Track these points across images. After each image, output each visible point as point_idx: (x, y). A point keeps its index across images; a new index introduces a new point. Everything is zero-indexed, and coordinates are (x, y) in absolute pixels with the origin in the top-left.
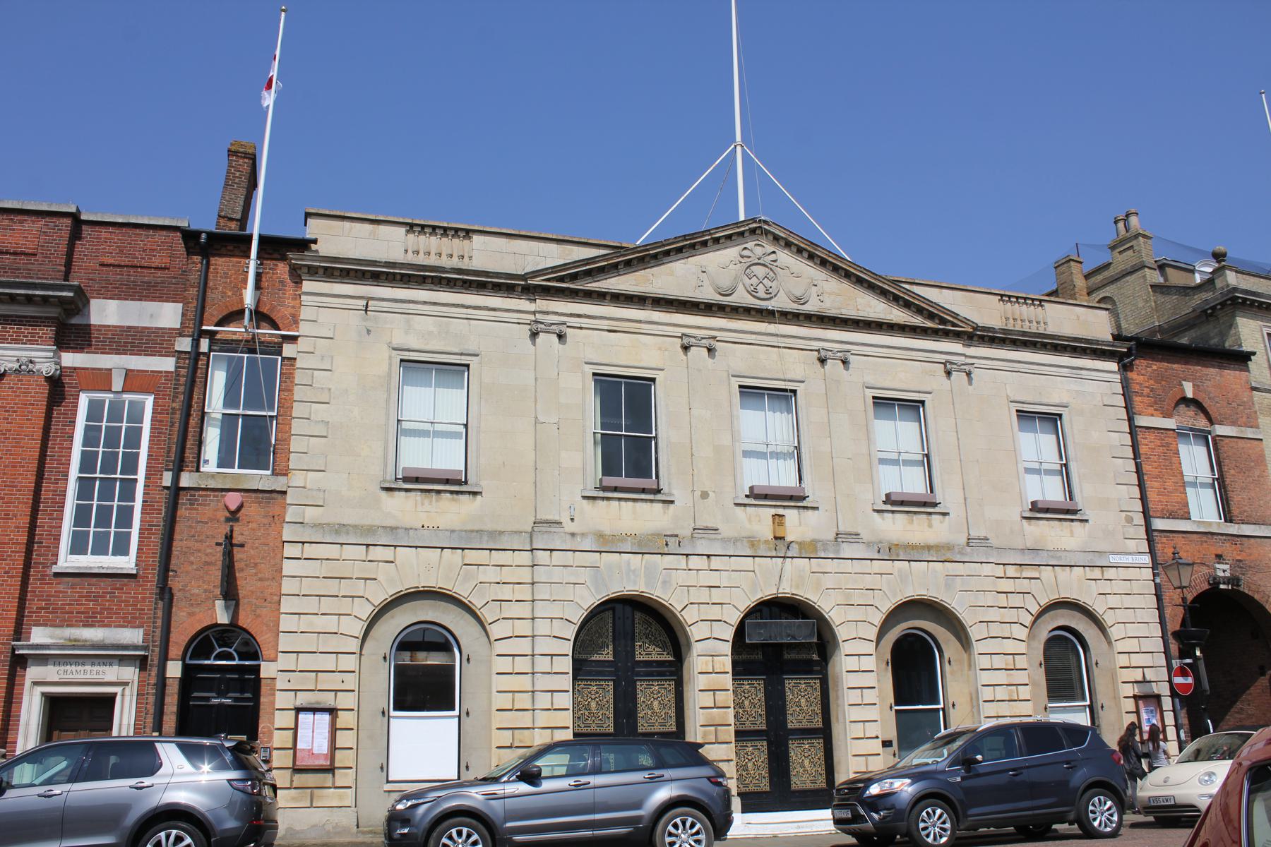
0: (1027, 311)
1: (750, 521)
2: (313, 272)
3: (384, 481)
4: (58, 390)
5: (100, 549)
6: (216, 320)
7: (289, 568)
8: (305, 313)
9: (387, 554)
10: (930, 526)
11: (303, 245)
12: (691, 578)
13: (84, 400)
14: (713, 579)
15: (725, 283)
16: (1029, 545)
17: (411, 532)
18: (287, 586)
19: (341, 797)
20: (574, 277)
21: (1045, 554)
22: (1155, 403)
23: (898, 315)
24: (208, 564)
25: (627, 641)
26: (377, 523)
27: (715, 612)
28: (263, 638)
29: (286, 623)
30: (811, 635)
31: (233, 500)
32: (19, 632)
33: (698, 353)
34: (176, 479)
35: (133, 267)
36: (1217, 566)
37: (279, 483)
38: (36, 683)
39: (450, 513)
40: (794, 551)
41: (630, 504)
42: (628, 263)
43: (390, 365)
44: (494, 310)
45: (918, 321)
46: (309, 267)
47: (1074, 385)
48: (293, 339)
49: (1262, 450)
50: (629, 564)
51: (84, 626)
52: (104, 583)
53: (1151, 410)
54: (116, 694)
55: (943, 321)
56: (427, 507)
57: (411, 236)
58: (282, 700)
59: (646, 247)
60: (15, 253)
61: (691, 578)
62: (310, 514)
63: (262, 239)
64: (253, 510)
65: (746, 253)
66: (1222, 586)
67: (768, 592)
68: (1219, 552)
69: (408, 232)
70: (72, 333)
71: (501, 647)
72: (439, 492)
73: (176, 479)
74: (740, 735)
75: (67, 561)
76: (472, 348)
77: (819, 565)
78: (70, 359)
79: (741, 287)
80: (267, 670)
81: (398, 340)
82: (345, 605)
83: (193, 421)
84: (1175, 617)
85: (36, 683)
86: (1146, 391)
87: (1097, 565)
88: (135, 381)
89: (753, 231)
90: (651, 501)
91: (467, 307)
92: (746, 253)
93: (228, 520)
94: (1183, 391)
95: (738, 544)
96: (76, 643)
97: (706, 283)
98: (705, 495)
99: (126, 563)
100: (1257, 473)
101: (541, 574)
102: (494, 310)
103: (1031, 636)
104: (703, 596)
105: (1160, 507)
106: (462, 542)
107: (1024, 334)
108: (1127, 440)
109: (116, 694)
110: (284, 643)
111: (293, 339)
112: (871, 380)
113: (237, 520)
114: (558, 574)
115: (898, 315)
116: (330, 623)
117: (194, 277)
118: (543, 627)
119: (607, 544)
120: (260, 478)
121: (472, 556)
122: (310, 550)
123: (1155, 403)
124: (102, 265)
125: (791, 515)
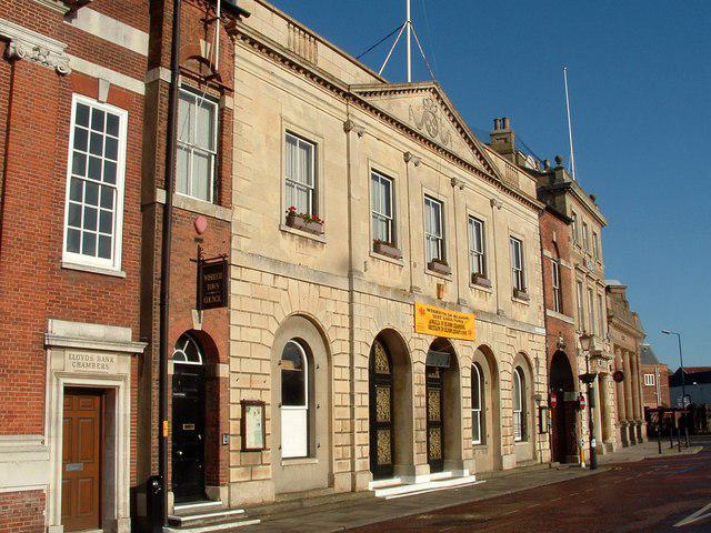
5: (89, 251)
19: (266, 472)
20: (365, 94)
24: (185, 276)
28: (219, 344)
29: (235, 333)
38: (60, 374)
45: (484, 169)
51: (88, 322)
52: (88, 275)
54: (119, 387)
55: (493, 173)
58: (235, 397)
80: (223, 371)
84: (550, 359)
87: (278, 266)
88: (117, 96)
99: (112, 265)
103: (278, 335)
109: (119, 387)
115: (478, 164)
120: (218, 212)
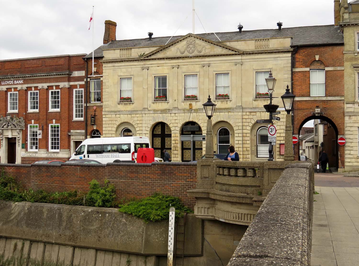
0: (263, 43)
1: (185, 105)
2: (104, 62)
3: (118, 102)
4: (71, 88)
6: (90, 74)
7: (104, 119)
8: (104, 71)
9: (119, 116)
10: (227, 104)
11: (102, 57)
12: (171, 118)
13: (74, 90)
14: (176, 118)
15: (182, 50)
16: (254, 107)
17: (122, 112)
18: (104, 123)
21: (258, 109)
22: (304, 63)
23: (225, 51)
25: (160, 131)
26: (117, 110)
27: (176, 125)
29: (104, 129)
30: (197, 129)
31: (95, 108)
32: (69, 131)
33: (176, 69)
34: (86, 105)
35: (79, 64)
36: (316, 109)
37: (101, 104)
39: (129, 107)
40: (193, 111)
41: (161, 103)
42: (164, 49)
43: (118, 80)
44: (136, 65)
46: (103, 62)
47: (275, 62)
48: (102, 77)
49: (343, 73)
50: (159, 116)
53: (302, 66)
56: (125, 106)
57: (121, 51)
59: (167, 45)
60: (61, 65)
61: (171, 118)
62: (107, 109)
63: (94, 58)
64: (98, 109)
65: (188, 42)
66: (316, 115)
67: (187, 120)
68: (318, 105)
69: (120, 51)
70: (70, 79)
71: (138, 132)
72: (127, 104)
73: (86, 105)
74: (170, 149)
75: (75, 119)
76: (132, 74)
77: (198, 114)
78: (72, 83)
79: (186, 51)
81: (119, 74)
82: (112, 126)
83: (88, 94)
85: (72, 139)
86: (301, 60)
89: (189, 36)
90: (258, 70)
91: (131, 66)
92: (188, 42)
93: (95, 111)
94: (315, 58)
95: (181, 111)
96: (76, 133)
97: (179, 51)
98: (175, 100)
100: (339, 80)
101: (143, 118)
102: (136, 65)
104: (174, 121)
105: (299, 94)
106: (131, 112)
107: (258, 51)
108: (290, 76)
110: (104, 132)
111: (102, 77)
112: (215, 69)
113: (96, 111)
114: (146, 118)
116: (110, 129)
117: (86, 66)
118: (144, 129)
119: (155, 111)
121: (133, 115)
122: (107, 116)
123: (304, 63)
124: (74, 64)
125: (194, 103)
